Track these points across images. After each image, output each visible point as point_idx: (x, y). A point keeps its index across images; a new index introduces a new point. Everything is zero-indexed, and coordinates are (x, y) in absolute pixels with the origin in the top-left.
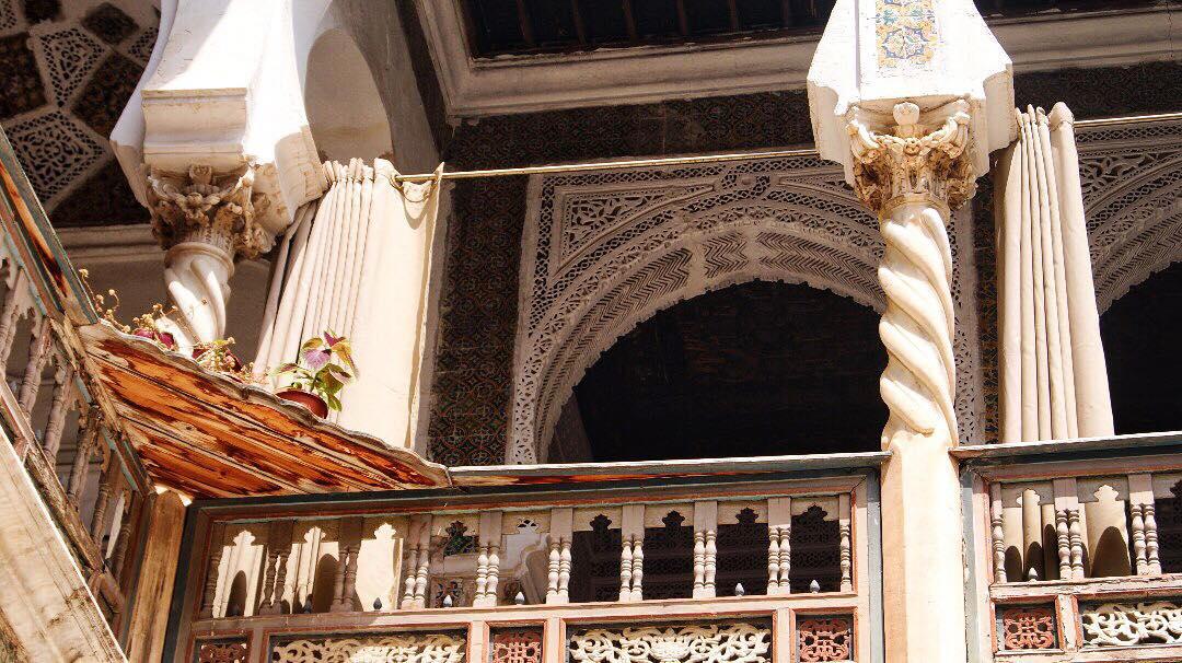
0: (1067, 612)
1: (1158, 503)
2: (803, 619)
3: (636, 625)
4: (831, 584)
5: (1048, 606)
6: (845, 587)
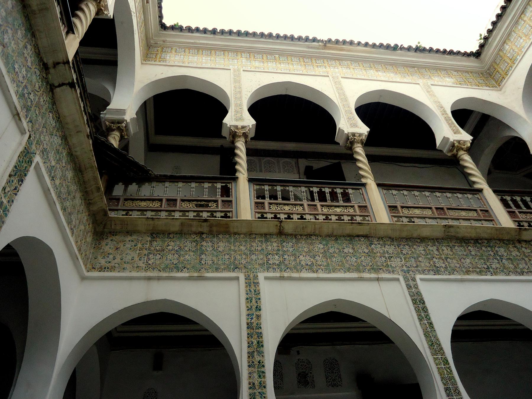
0: (266, 205)
1: (341, 192)
2: (223, 201)
3: (280, 204)
4: (228, 196)
5: (263, 203)
6: (231, 197)
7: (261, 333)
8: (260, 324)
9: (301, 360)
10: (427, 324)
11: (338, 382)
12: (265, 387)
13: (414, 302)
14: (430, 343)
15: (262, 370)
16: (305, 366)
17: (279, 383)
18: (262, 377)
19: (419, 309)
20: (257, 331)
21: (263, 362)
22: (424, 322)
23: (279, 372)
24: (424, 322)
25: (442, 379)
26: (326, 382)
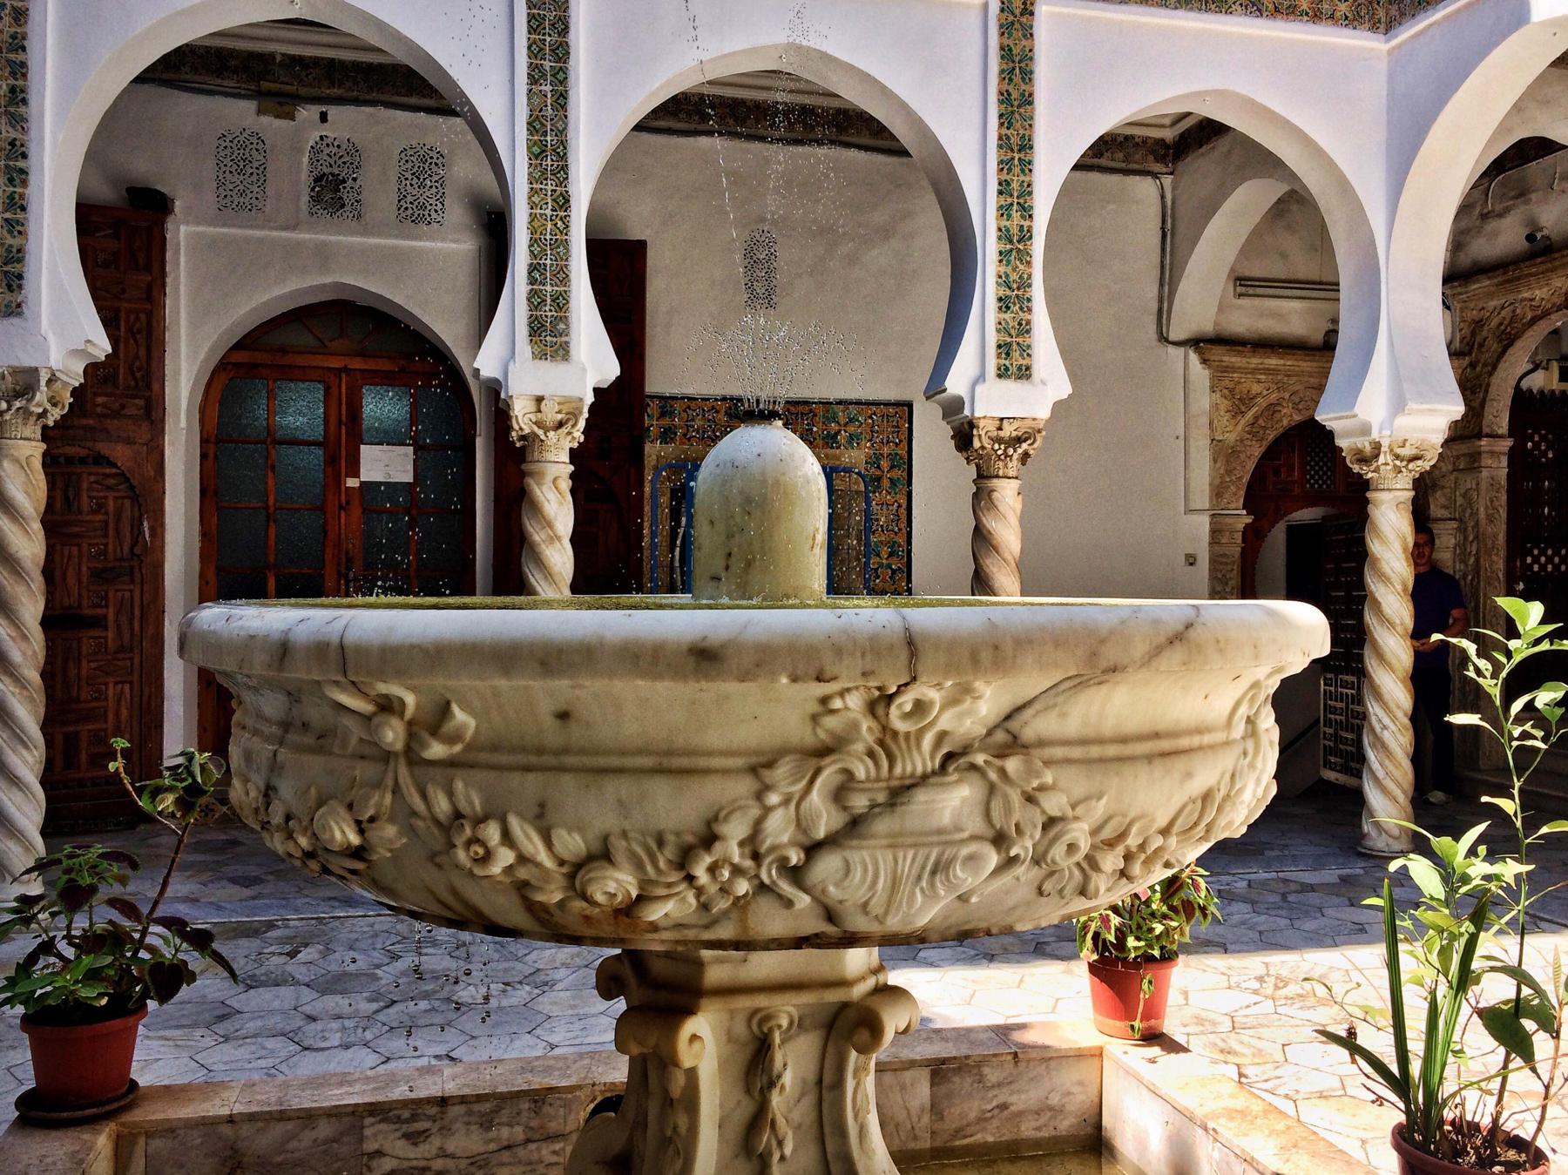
7: (23, 65)
8: (24, 38)
9: (329, 141)
10: (549, 95)
11: (433, 213)
12: (23, 209)
13: (534, 24)
14: (536, 150)
15: (21, 164)
16: (341, 157)
17: (254, 195)
18: (17, 181)
19: (541, 50)
20: (12, 56)
21: (22, 145)
22: (543, 88)
23: (256, 164)
24: (543, 88)
25: (533, 242)
26: (395, 208)
